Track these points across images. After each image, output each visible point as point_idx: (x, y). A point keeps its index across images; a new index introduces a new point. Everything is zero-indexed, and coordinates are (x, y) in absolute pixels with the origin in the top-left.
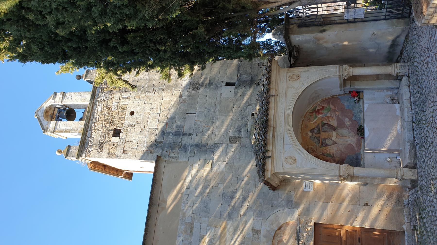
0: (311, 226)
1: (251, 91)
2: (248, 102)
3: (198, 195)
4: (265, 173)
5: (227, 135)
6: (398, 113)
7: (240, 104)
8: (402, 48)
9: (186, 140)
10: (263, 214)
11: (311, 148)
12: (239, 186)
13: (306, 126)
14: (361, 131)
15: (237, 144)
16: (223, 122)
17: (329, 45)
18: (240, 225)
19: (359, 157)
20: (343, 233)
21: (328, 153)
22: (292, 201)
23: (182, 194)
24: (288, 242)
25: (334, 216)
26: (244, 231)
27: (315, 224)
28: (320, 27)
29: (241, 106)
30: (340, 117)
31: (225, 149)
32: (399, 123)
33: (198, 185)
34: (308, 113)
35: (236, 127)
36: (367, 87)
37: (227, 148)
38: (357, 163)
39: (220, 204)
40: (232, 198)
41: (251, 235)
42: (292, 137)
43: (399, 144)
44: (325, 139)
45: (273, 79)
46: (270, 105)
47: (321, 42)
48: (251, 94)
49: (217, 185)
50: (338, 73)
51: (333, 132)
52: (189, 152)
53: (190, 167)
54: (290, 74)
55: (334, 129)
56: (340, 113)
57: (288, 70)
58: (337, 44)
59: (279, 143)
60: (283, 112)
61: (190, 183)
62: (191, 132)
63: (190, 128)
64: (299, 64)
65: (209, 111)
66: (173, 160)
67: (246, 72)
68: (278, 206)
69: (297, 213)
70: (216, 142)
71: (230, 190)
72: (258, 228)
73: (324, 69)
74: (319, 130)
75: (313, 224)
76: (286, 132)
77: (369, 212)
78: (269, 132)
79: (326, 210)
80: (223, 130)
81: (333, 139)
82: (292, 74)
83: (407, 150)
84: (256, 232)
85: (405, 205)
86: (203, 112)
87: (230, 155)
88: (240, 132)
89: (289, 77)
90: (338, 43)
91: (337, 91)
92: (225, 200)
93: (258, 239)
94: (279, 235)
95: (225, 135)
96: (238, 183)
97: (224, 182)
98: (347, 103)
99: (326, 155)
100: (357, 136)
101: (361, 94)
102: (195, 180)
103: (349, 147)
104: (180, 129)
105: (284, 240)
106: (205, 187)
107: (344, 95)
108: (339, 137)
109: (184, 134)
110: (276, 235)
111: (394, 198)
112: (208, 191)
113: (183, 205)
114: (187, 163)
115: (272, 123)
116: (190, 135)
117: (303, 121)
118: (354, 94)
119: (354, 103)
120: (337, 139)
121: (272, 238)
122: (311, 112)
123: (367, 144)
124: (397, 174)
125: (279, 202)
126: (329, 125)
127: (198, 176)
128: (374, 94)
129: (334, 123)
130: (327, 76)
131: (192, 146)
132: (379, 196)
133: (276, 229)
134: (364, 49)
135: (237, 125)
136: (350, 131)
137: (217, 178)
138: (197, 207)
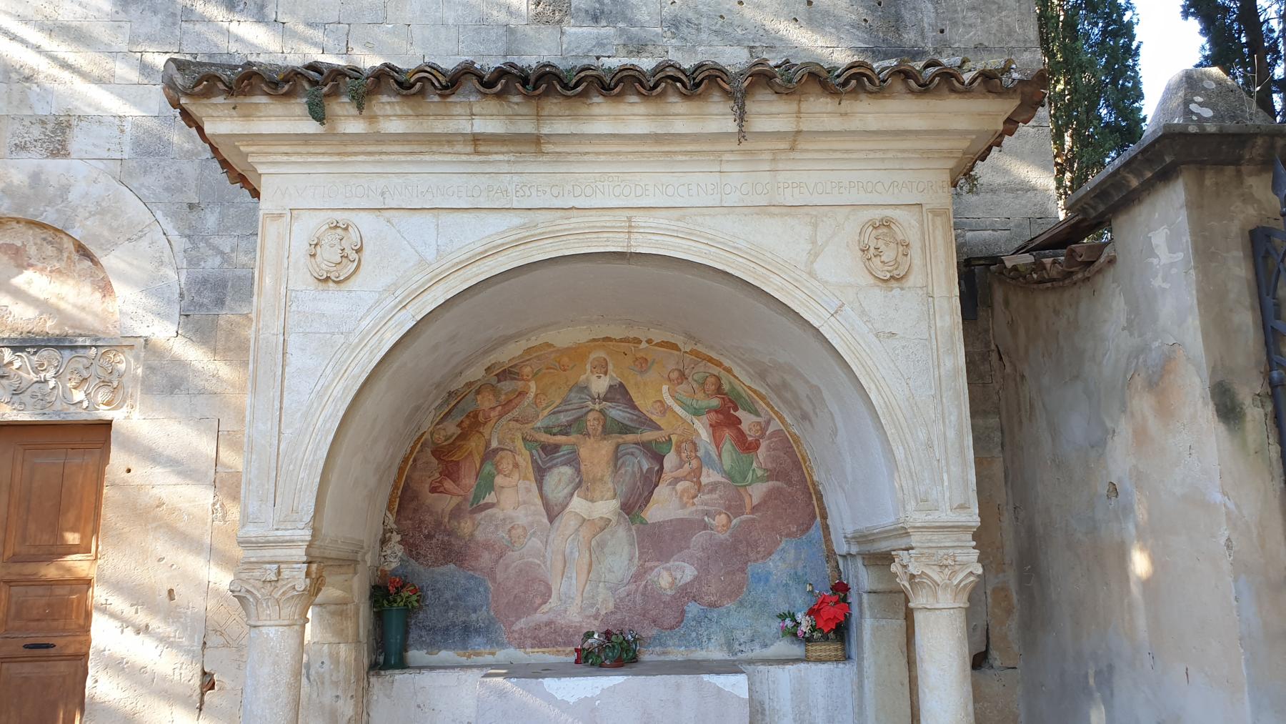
0: (92, 407)
4: (220, 100)
10: (151, 161)
11: (522, 394)
12: (295, 35)
13: (643, 364)
14: (613, 651)
17: (1120, 461)
18: (92, 55)
20: (78, 564)
21: (499, 480)
22: (220, 302)
24: (18, 294)
25: (149, 516)
26: (66, 75)
27: (98, 434)
28: (1259, 386)
30: (699, 538)
34: (716, 370)
36: (869, 685)
38: (447, 629)
41: (41, 110)
42: (484, 256)
44: (573, 460)
45: (869, 113)
46: (677, 105)
47: (1143, 404)
50: (919, 518)
51: (614, 504)
54: (908, 226)
55: (632, 507)
56: (723, 536)
57: (935, 213)
58: (1127, 510)
60: (642, 194)
64: (1007, 303)
67: (954, 23)
68: (192, 235)
69: (163, 332)
72: (78, 141)
73: (951, 434)
74: (625, 429)
75: (104, 413)
76: (516, 220)
77: (168, 694)
78: (492, 105)
79: (173, 479)
82: (913, 236)
84: (57, 134)
88: (596, 19)
89: (886, 224)
90: (1141, 513)
91: (845, 519)
93: (22, 147)
94: (49, 250)
96: (310, 25)
98: (784, 573)
99: (488, 467)
100: (595, 626)
101: (830, 649)
103: (535, 588)
105: (29, 274)
107: (831, 555)
108: (585, 532)
110: (48, 234)
115: (561, 127)
117: (674, 347)
118: (830, 610)
119: (784, 608)
120: (573, 523)
121: (31, 213)
122: (726, 387)
123: (502, 694)
125: (216, 241)
126: (650, 482)
129: (664, 506)
130: (899, 453)
133: (77, 233)
134: (1106, 676)
136: (622, 591)
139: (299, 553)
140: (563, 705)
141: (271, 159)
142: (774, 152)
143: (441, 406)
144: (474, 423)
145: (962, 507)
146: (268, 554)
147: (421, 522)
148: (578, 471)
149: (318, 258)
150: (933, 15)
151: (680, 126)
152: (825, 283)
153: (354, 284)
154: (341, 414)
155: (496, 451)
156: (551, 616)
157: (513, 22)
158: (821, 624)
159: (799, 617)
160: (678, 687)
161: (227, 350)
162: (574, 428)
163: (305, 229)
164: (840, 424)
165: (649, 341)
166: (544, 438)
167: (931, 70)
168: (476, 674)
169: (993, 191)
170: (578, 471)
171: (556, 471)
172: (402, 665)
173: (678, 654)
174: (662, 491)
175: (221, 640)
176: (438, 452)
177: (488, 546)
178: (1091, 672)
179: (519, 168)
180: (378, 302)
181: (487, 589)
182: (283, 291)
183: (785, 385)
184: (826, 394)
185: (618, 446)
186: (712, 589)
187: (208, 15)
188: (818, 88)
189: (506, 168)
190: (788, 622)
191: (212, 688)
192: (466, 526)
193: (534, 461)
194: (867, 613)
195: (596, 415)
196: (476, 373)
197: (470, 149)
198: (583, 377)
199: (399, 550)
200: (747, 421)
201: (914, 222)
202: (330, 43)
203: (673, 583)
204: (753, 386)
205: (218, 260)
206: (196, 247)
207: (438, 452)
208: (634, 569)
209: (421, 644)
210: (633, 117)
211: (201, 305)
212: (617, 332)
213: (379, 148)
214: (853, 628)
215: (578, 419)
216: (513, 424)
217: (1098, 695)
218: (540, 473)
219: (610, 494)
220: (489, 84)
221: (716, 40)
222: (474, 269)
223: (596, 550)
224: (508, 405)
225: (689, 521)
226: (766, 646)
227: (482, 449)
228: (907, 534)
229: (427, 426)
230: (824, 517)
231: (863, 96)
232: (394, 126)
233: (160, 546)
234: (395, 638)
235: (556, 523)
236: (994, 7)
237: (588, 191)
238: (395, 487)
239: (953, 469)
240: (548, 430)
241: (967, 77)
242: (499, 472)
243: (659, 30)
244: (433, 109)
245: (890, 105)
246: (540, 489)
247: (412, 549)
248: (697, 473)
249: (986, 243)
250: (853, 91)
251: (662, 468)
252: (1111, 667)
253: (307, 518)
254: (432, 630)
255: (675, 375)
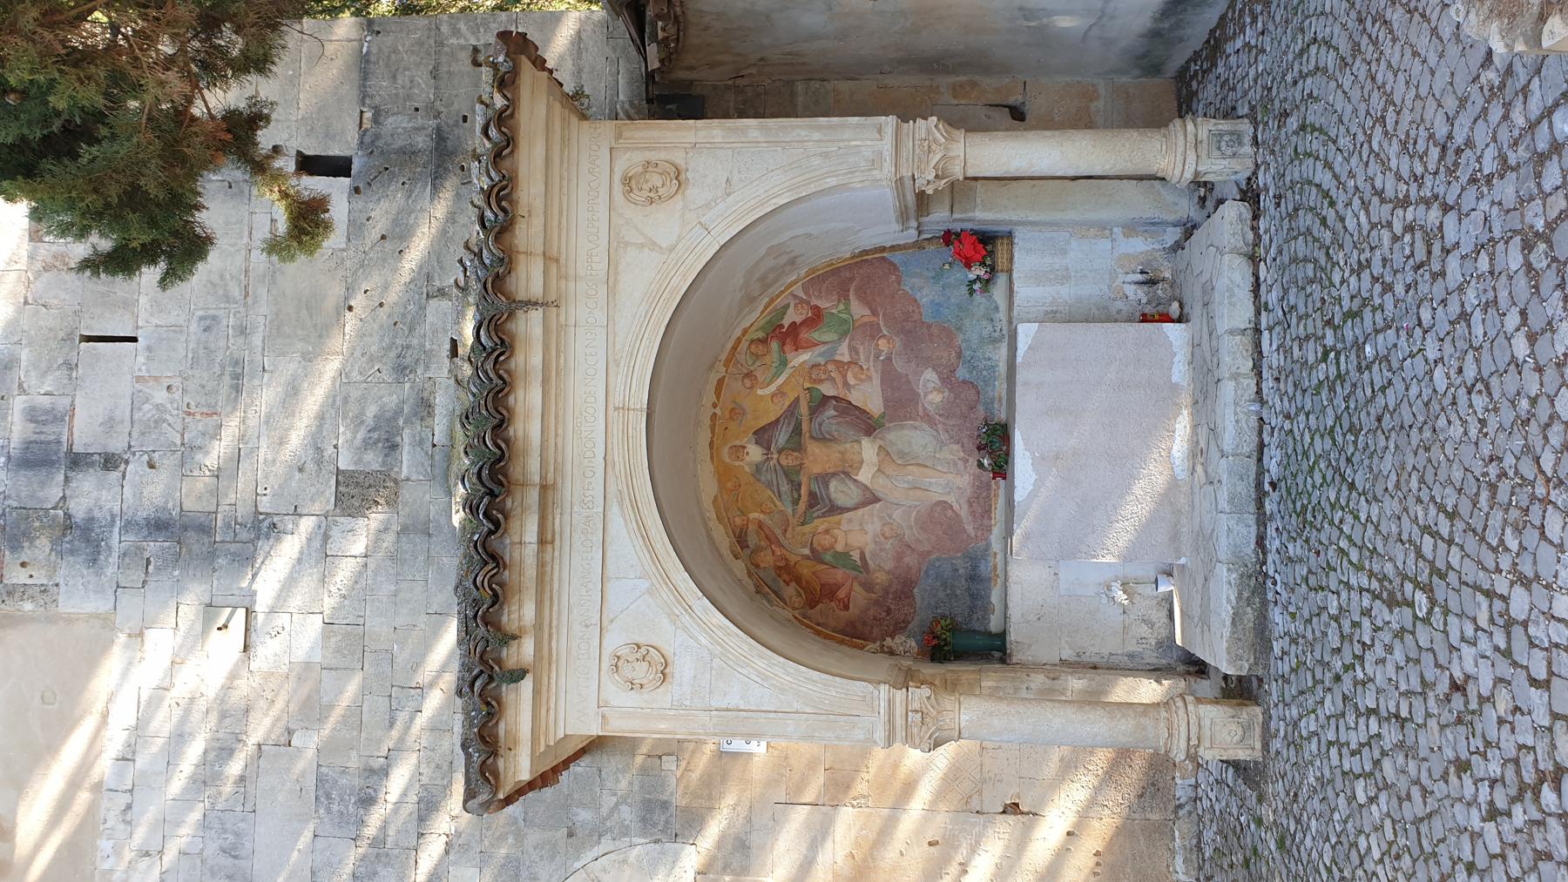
1: (440, 209)
2: (429, 278)
3: (185, 790)
4: (501, 763)
5: (319, 463)
6: (1180, 372)
7: (386, 287)
8: (1223, 18)
9: (90, 495)
10: (524, 874)
11: (760, 525)
12: (401, 740)
13: (736, 412)
14: (995, 445)
15: (376, 518)
16: (293, 392)
19: (983, 569)
21: (839, 548)
22: (665, 805)
23: (98, 787)
29: (392, 297)
30: (899, 365)
31: (317, 544)
32: (1183, 425)
33: (180, 738)
34: (744, 344)
35: (370, 422)
36: (1033, 217)
37: (326, 538)
39: (307, 836)
40: (367, 801)
42: (646, 538)
43: (1175, 537)
44: (824, 479)
45: (530, 192)
46: (518, 361)
48: (443, 232)
49: (283, 740)
52: (114, 559)
53: (126, 646)
54: (629, 161)
55: (869, 426)
56: (898, 343)
57: (619, 136)
59: (576, 570)
61: (139, 730)
62: (117, 445)
63: (110, 423)
64: (691, 68)
65: (209, 324)
66: (28, 606)
67: (408, 97)
68: (598, 833)
70: (265, 505)
71: (354, 762)
73: (817, 136)
74: (797, 431)
76: (614, 509)
77: (1021, 844)
78: (514, 524)
79: (829, 845)
80: (297, 438)
81: (864, 476)
83: (1226, 612)
85: (1180, 806)
86: (177, 329)
87: (344, 572)
88: (394, 447)
89: (627, 181)
91: (886, 231)
92: (329, 811)
95: (310, 466)
96: (392, 725)
97: (322, 719)
98: (933, 288)
99: (828, 557)
101: (1001, 249)
102: (162, 714)
104: (48, 429)
106: (222, 751)
107: (918, 245)
108: (890, 470)
109: (77, 461)
111: (1133, 776)
112: (235, 767)
113: (105, 845)
114: (107, 623)
115: (534, 465)
116: (110, 462)
117: (720, 382)
118: (966, 248)
119: (964, 290)
120: (882, 480)
122: (761, 335)
123: (1027, 537)
124: (1170, 735)
125: (605, 811)
126: (847, 409)
127: (170, 698)
128: (1064, 252)
129: (869, 396)
130: (832, 182)
131: (128, 526)
132: (1068, 768)
134: (1028, 14)
135: (371, 411)
136: (944, 436)
137: (280, 704)
138: (183, 853)
139: (900, 695)
140: (1038, 485)
141: (552, 725)
142: (559, 277)
143: (769, 601)
144: (786, 570)
145: (880, 131)
146: (899, 722)
147: (875, 619)
148: (834, 474)
149: (644, 681)
150: (400, 118)
151: (536, 359)
152: (680, 239)
153: (669, 653)
154: (782, 660)
155: (813, 550)
156: (963, 501)
157: (396, 527)
158: (978, 256)
159: (972, 276)
160: (1026, 384)
161: (710, 797)
162: (794, 478)
163: (619, 697)
164: (800, 231)
165: (715, 405)
166: (802, 505)
167: (493, 132)
168: (1012, 568)
169: (580, 71)
170: (834, 474)
171: (833, 495)
172: (1002, 635)
173: (1001, 387)
174: (855, 398)
175: (975, 798)
176: (812, 603)
177: (899, 558)
178: (1025, 23)
179: (567, 505)
180: (685, 629)
181: (938, 559)
182: (672, 713)
183: (762, 279)
184: (775, 242)
185: (812, 437)
186: (946, 354)
187: (379, 823)
188: (507, 236)
189: (567, 517)
190: (977, 286)
191: (1017, 805)
192: (881, 578)
193: (824, 515)
194: (970, 215)
195: (783, 457)
196: (739, 568)
197: (549, 548)
198: (747, 469)
199: (899, 639)
200: (793, 316)
201: (628, 155)
202: (412, 705)
203: (939, 391)
204: (761, 308)
205: (623, 808)
206: (610, 830)
207: (812, 603)
208: (925, 426)
209: (986, 619)
210: (528, 401)
211: (667, 822)
212: (704, 436)
213: (546, 629)
214: (983, 228)
215: (786, 475)
216: (788, 535)
217: (1045, 21)
218: (835, 509)
219: (856, 445)
220: (497, 524)
221: (419, 331)
222: (658, 546)
223: (905, 459)
224: (771, 539)
225: (883, 373)
226: (997, 308)
227: (809, 563)
228: (901, 178)
229: (787, 613)
230: (883, 249)
231: (514, 196)
232: (529, 612)
233: (890, 855)
234: (980, 641)
235: (880, 495)
236: (393, 57)
237: (589, 445)
238: (842, 642)
239: (846, 136)
240: (796, 502)
241: (499, 102)
242: (832, 547)
243: (407, 386)
244: (515, 577)
245: (523, 171)
246: (849, 510)
247: (899, 627)
248: (840, 365)
249: (630, 82)
250: (511, 203)
251: (834, 397)
252: (1021, 9)
253: (871, 687)
254: (973, 609)
255: (748, 382)
